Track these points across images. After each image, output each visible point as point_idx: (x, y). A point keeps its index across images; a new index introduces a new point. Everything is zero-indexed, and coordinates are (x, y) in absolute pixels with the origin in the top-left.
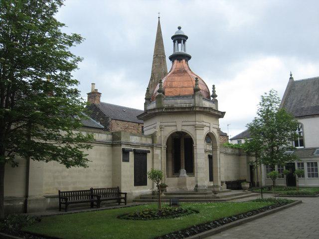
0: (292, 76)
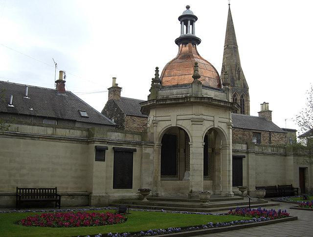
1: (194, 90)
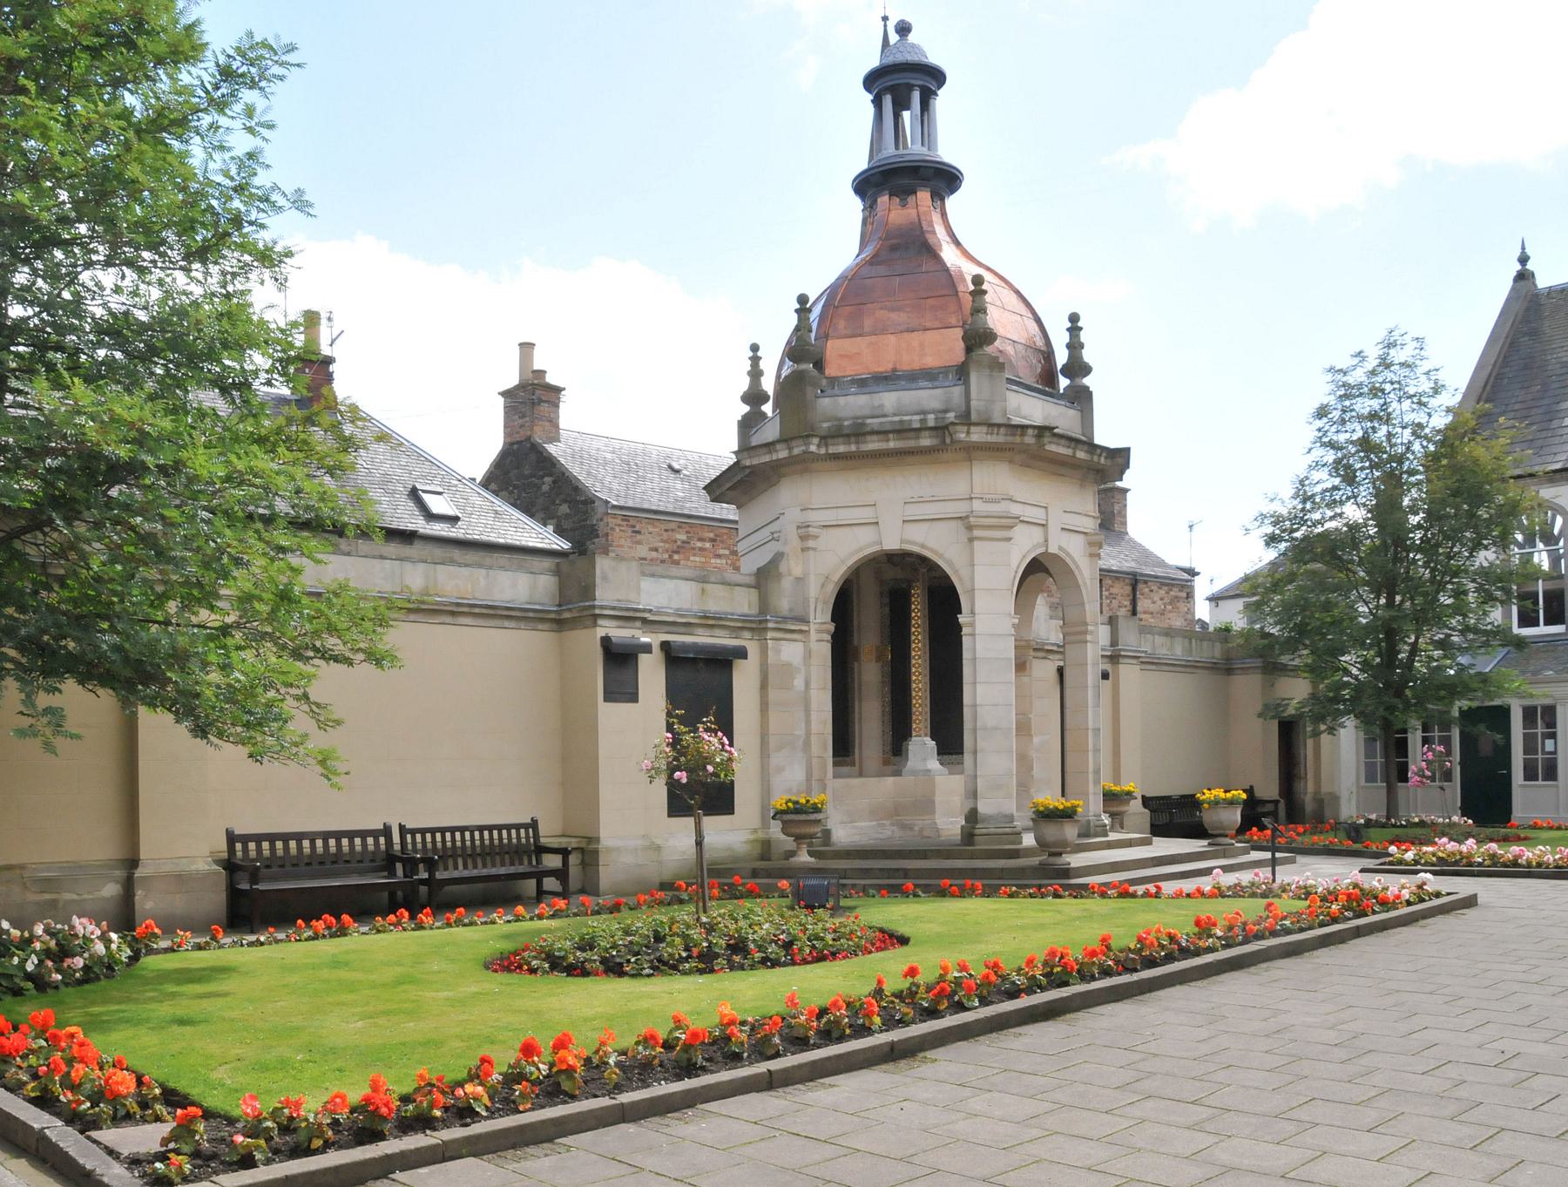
0: (1530, 266)
1: (974, 394)
